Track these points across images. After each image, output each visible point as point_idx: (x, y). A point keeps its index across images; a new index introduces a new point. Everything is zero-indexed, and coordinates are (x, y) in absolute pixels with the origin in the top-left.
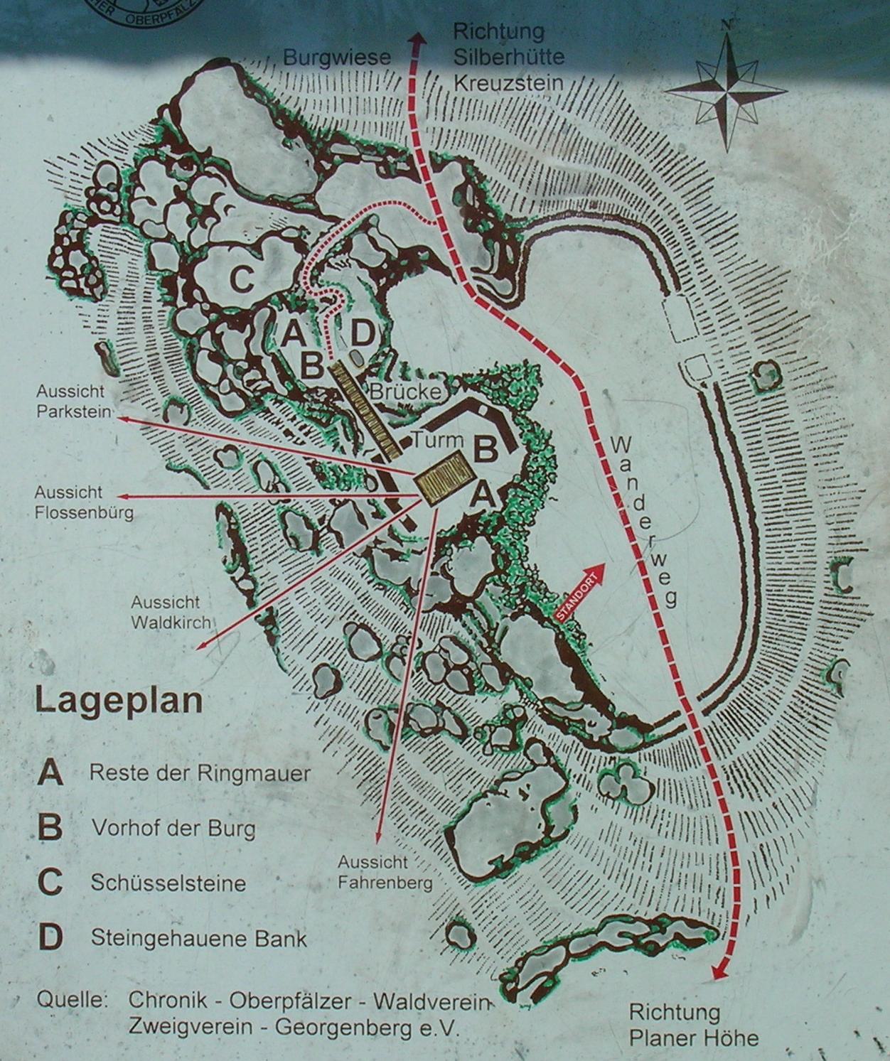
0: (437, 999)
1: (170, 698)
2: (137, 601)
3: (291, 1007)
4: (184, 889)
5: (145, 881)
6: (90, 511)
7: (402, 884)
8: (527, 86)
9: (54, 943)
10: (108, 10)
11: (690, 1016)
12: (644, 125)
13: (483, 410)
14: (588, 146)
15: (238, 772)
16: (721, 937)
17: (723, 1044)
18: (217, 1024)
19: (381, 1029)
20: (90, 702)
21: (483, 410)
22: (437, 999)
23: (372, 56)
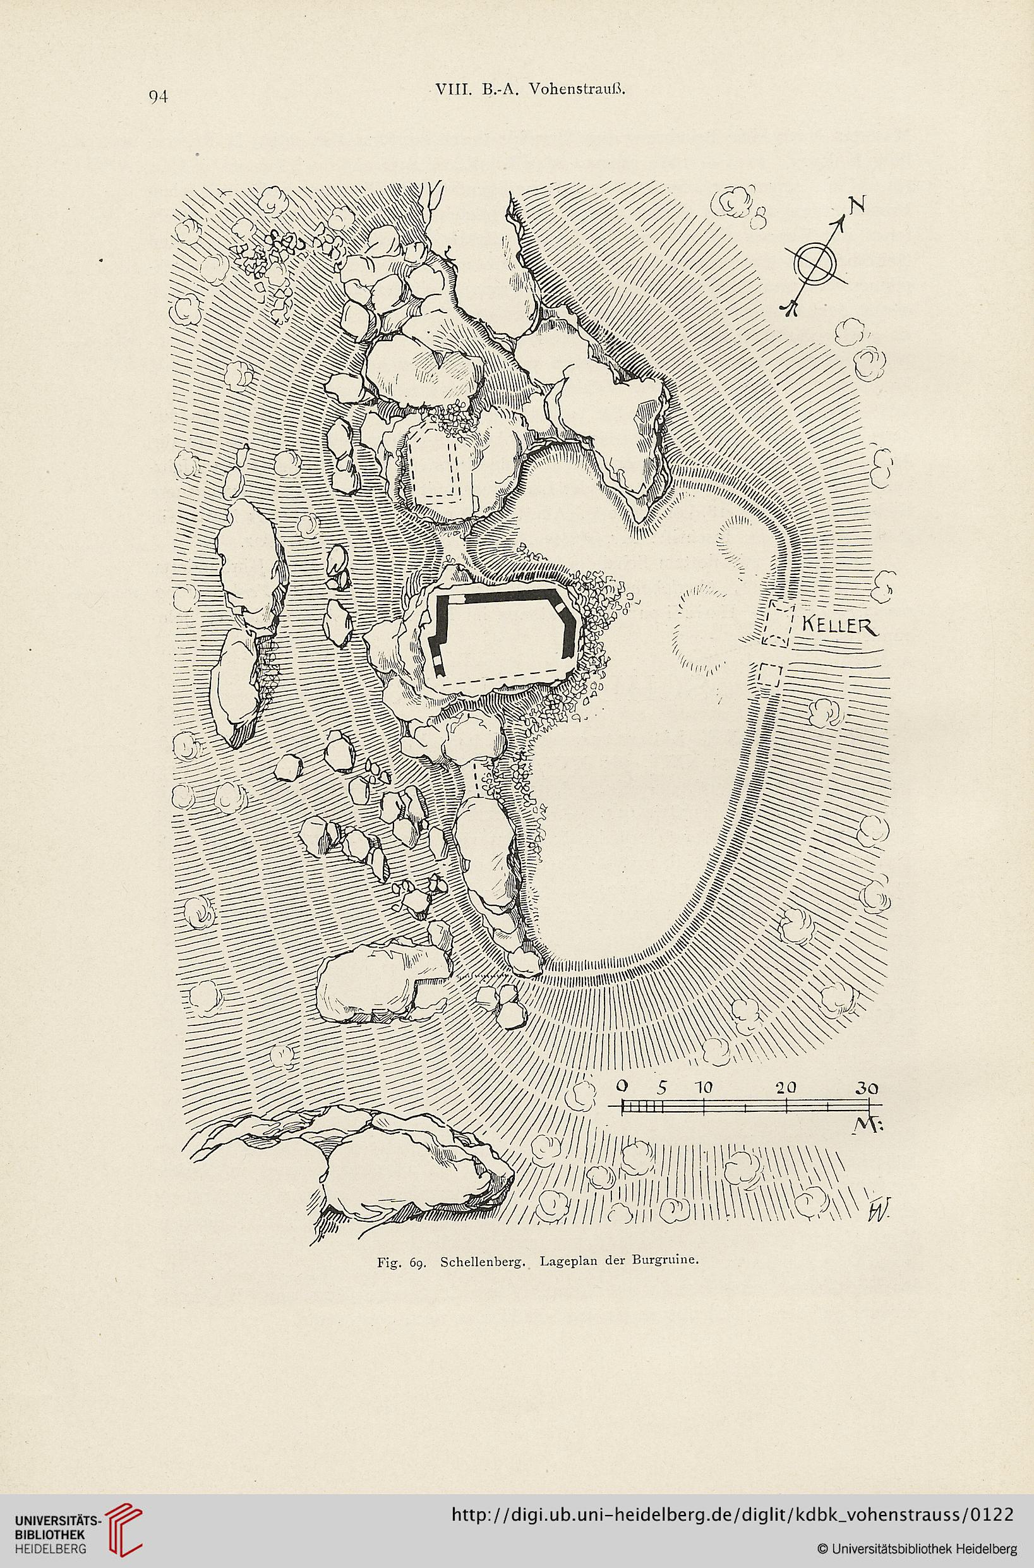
0: (855, 1512)
1: (927, 1514)
2: (80, 1521)
3: (761, 1513)
4: (67, 1518)
5: (945, 1513)
6: (891, 1513)
7: (672, 1516)
8: (908, 1517)
9: (567, 1518)
10: (53, 1521)
11: (647, 1518)
12: (779, 1511)
13: (560, 608)
14: (772, 517)
15: (764, 1514)
16: (856, 1514)
17: (864, 1513)
18: (690, 1513)
19: (679, 1516)
20: (533, 1516)
21: (560, 608)
22: (855, 1512)
23: (93, 1518)
